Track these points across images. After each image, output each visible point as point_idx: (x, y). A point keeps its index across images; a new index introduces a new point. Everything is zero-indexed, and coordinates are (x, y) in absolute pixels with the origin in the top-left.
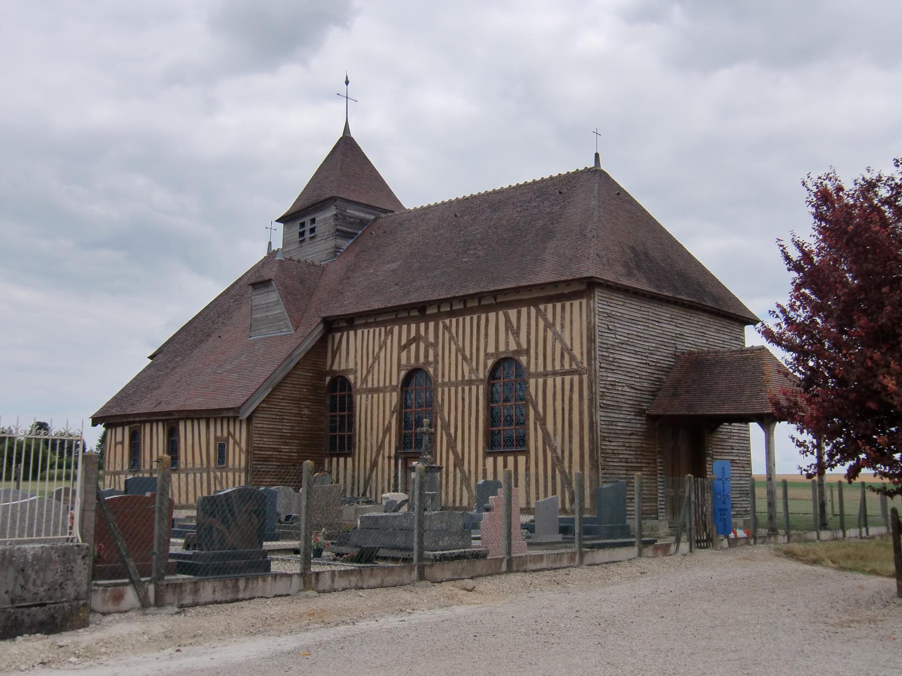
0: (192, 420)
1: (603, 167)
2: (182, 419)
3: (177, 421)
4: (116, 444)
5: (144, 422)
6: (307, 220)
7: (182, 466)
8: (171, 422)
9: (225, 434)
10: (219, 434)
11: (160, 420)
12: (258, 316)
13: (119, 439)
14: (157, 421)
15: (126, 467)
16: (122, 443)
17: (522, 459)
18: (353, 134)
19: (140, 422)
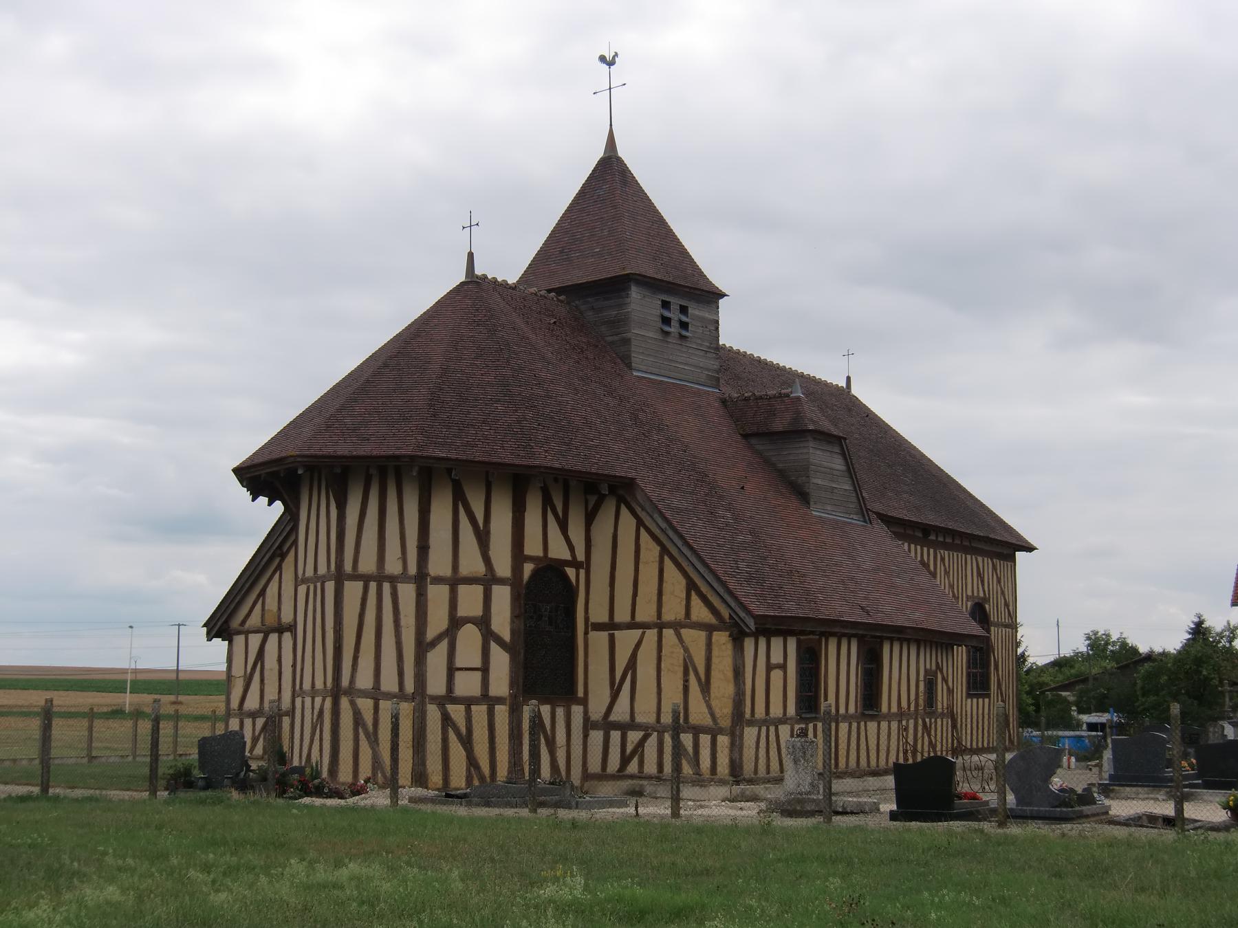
0: (901, 641)
1: (855, 391)
2: (888, 638)
3: (881, 640)
4: (770, 668)
5: (827, 635)
6: (675, 302)
7: (884, 709)
8: (873, 641)
9: (934, 667)
10: (928, 666)
11: (844, 635)
12: (819, 482)
13: (777, 658)
14: (849, 637)
15: (791, 711)
16: (783, 667)
17: (987, 700)
18: (621, 153)
19: (822, 634)
